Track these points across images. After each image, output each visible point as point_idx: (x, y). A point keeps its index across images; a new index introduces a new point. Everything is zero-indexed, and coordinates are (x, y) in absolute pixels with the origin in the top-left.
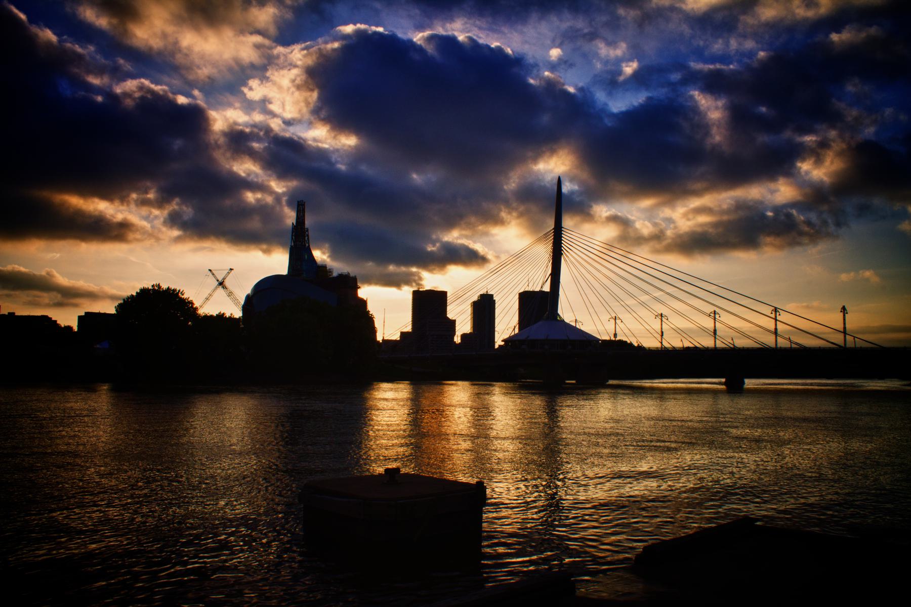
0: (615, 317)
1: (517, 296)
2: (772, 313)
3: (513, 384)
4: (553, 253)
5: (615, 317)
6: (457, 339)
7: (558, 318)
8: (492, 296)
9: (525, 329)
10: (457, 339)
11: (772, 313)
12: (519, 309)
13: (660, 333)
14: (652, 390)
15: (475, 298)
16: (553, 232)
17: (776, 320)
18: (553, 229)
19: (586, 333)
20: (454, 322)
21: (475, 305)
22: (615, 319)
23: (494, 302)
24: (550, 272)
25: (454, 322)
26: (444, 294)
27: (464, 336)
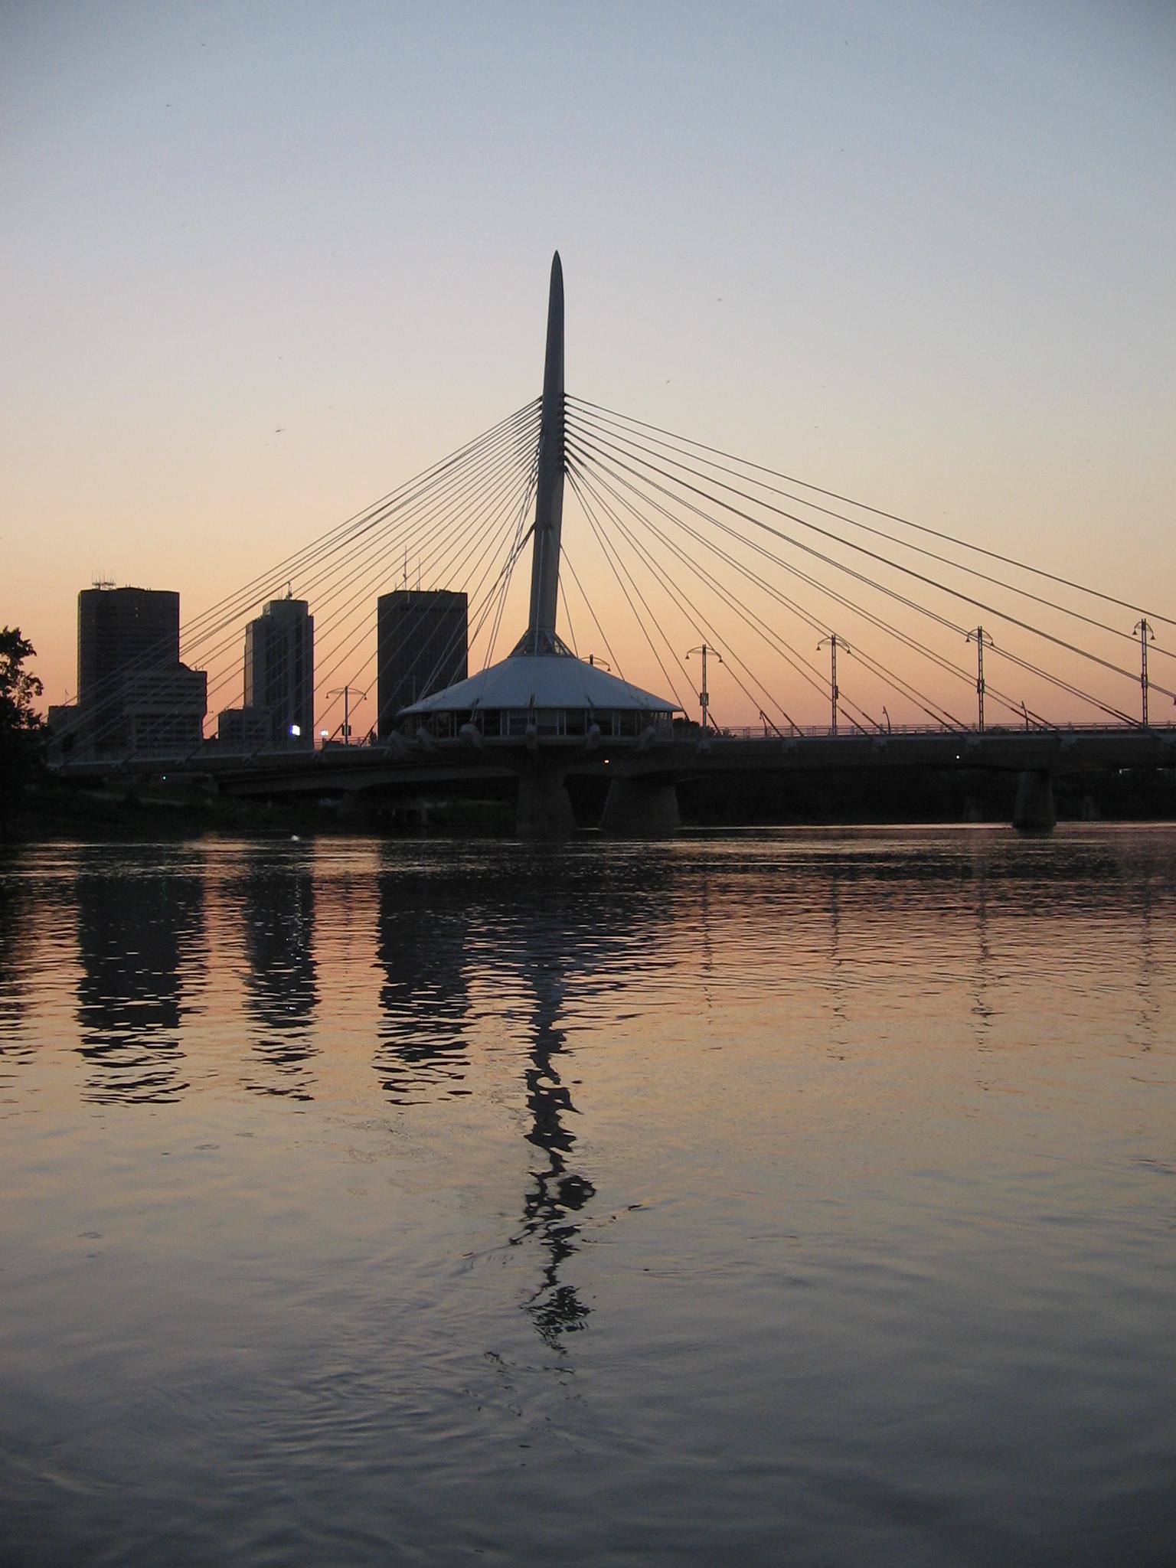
0: (704, 648)
1: (374, 604)
2: (1135, 633)
3: (387, 854)
4: (539, 473)
5: (704, 648)
6: (210, 728)
7: (557, 650)
8: (303, 604)
9: (456, 683)
10: (210, 728)
11: (1135, 633)
12: (379, 651)
13: (829, 691)
14: (747, 865)
15: (257, 613)
16: (540, 408)
17: (1144, 644)
18: (540, 399)
19: (637, 689)
20: (202, 676)
21: (258, 629)
22: (704, 652)
23: (398, 594)
24: (531, 519)
25: (202, 676)
26: (178, 594)
27: (228, 718)
